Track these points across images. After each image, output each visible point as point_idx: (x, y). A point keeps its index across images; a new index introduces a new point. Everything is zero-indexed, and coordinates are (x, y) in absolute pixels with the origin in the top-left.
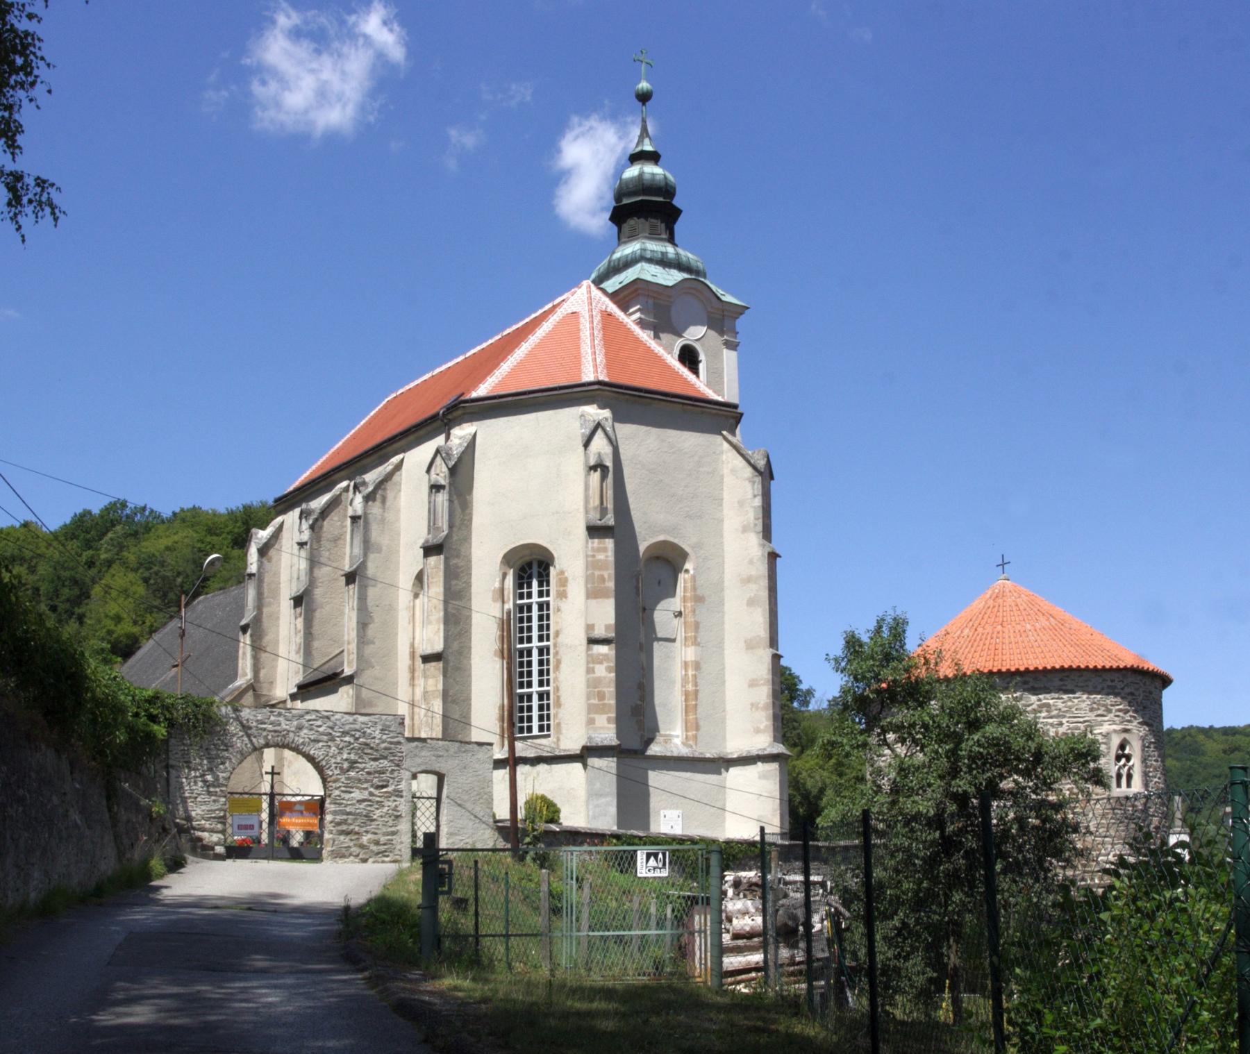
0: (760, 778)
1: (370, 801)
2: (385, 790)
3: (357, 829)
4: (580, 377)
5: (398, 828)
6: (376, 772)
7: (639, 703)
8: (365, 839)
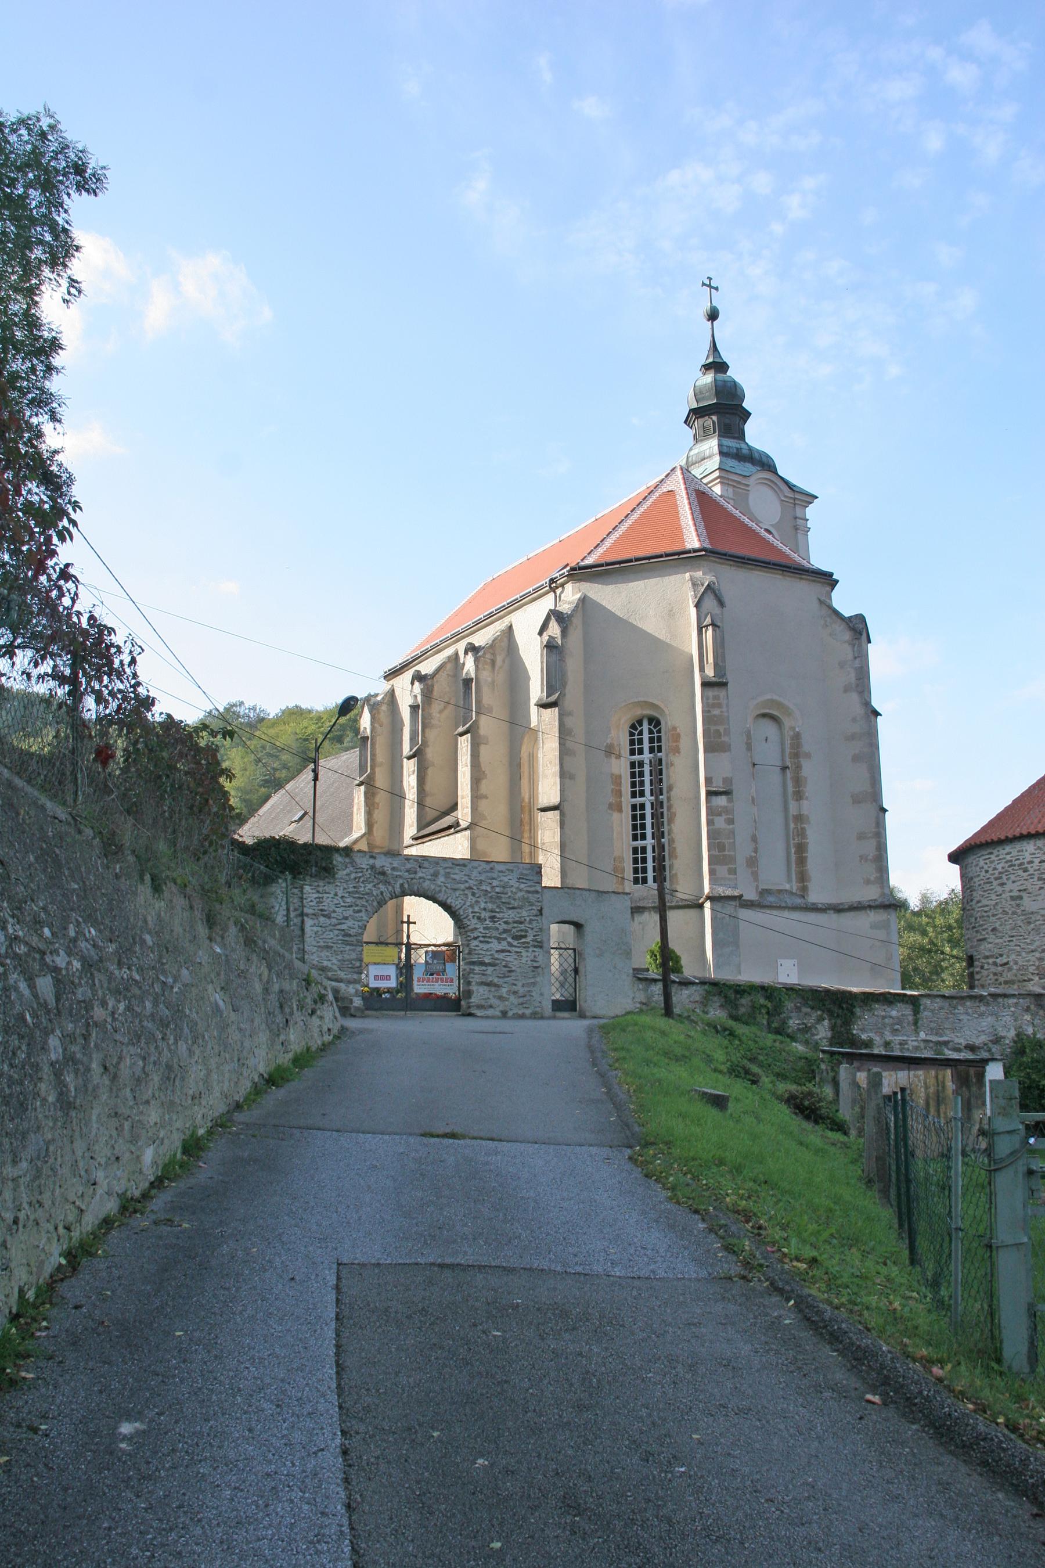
0: (871, 927)
1: (509, 951)
2: (523, 940)
3: (496, 980)
4: (684, 545)
5: (538, 979)
6: (515, 922)
7: (753, 854)
8: (504, 991)
